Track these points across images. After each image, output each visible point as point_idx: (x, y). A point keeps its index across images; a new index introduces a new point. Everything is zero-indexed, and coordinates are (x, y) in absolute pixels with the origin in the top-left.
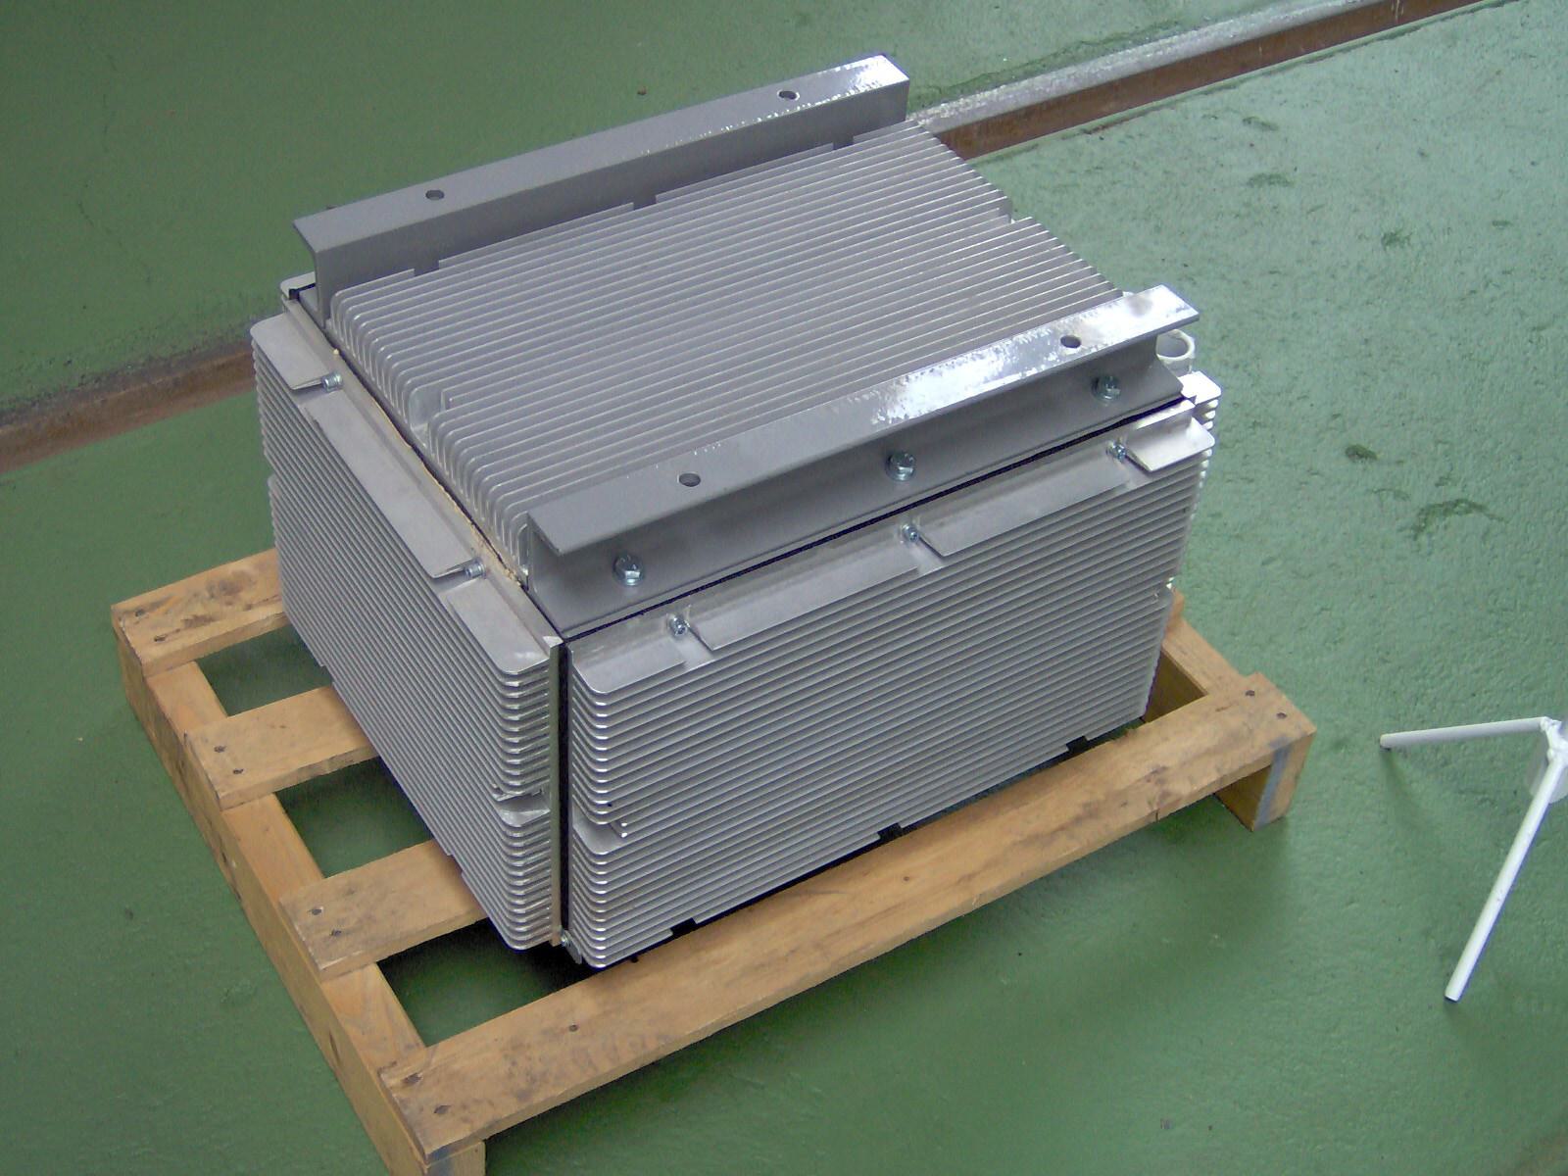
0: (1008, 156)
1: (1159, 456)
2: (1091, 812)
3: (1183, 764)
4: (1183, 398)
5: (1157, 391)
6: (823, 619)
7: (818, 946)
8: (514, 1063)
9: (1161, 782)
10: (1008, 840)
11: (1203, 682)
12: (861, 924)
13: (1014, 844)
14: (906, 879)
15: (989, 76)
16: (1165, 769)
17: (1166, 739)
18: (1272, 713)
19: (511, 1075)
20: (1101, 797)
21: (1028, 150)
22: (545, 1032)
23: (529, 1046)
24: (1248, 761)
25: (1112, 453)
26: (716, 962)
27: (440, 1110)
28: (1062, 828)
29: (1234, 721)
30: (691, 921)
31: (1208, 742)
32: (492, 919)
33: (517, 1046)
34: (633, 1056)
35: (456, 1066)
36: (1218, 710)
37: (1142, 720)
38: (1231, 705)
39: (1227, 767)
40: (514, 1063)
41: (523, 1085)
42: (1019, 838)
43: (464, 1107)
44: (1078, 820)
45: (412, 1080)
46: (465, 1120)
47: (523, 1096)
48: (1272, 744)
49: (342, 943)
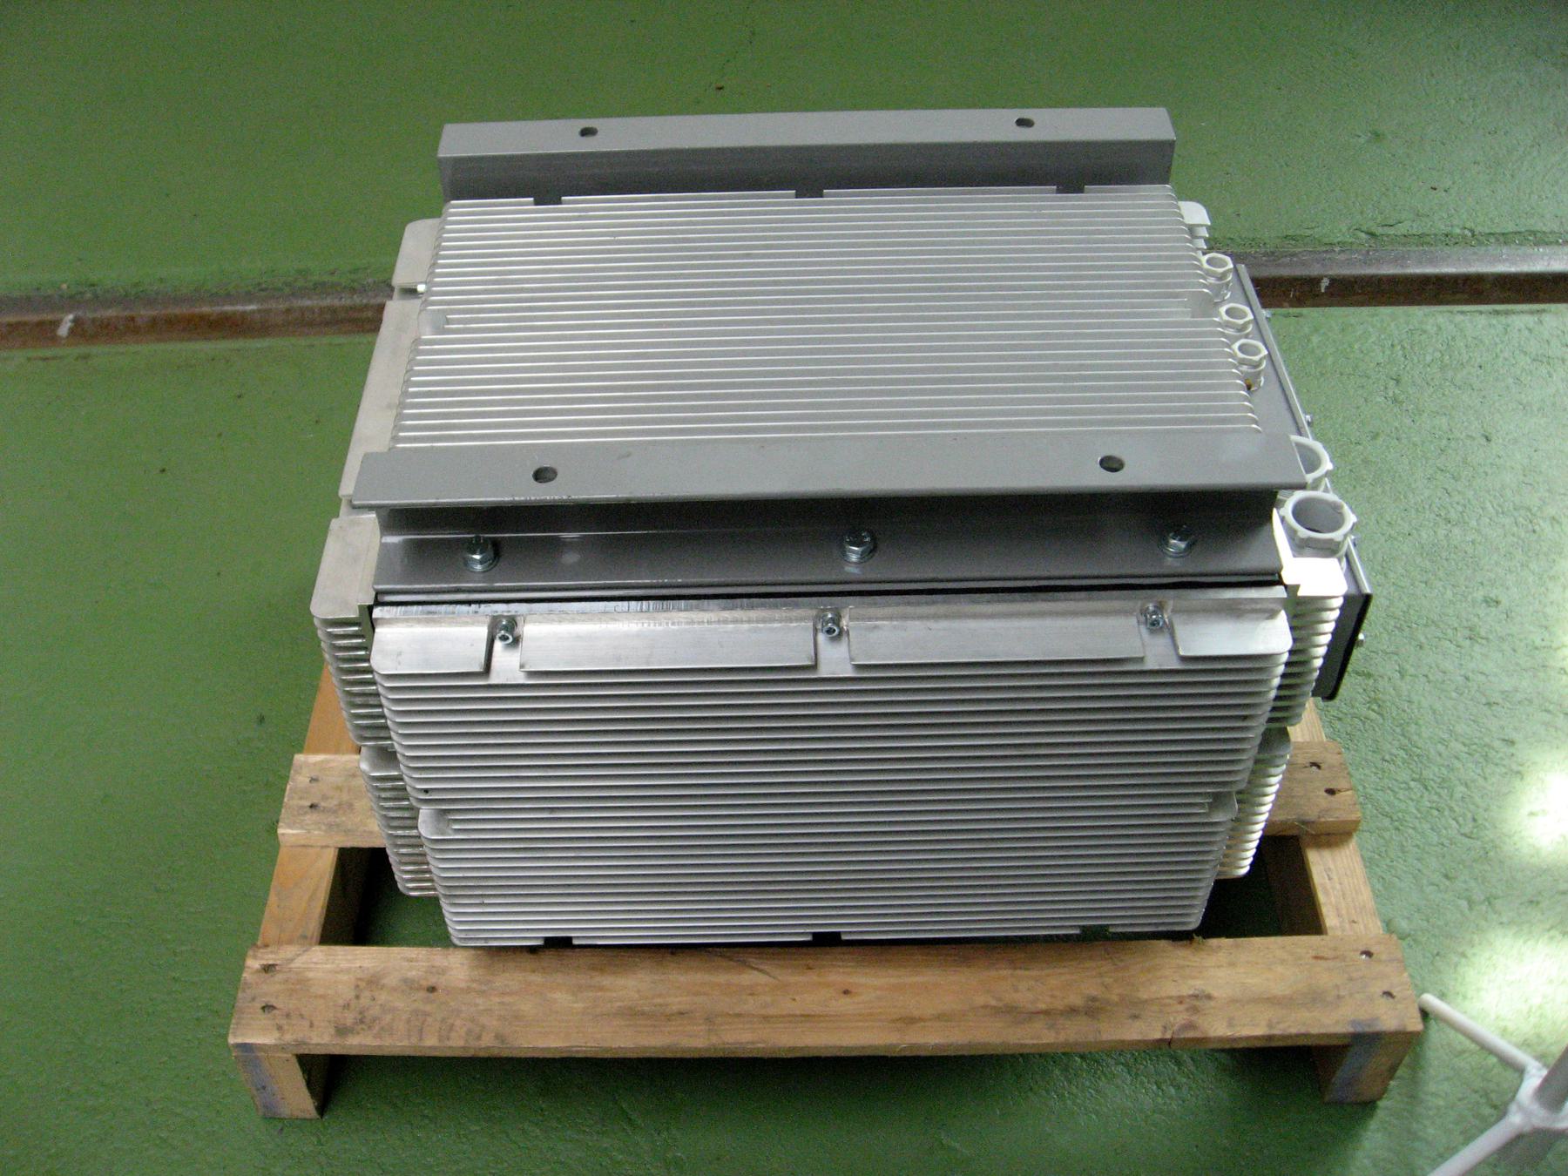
0: (1507, 313)
1: (1214, 637)
2: (1093, 1009)
3: (1233, 1001)
4: (1280, 582)
5: (1248, 559)
6: (1034, 699)
7: (709, 1020)
8: (357, 997)
9: (1195, 1010)
10: (980, 1000)
11: (1330, 919)
12: (766, 1018)
13: (985, 1007)
14: (846, 992)
15: (1534, 233)
16: (1209, 997)
17: (1232, 964)
18: (1377, 988)
19: (347, 1006)
20: (1115, 998)
21: (1532, 313)
22: (405, 981)
23: (383, 987)
24: (1314, 1031)
25: (1144, 612)
26: (601, 989)
27: (267, 1008)
28: (1047, 1013)
29: (1326, 978)
30: (570, 939)
31: (1279, 989)
32: (349, 844)
33: (373, 981)
34: (461, 1043)
35: (310, 975)
36: (1316, 958)
37: (1180, 937)
38: (1335, 958)
39: (1282, 1026)
40: (357, 997)
41: (349, 1022)
42: (993, 1003)
43: (288, 1016)
44: (1072, 1011)
45: (268, 969)
46: (280, 1028)
47: (342, 1031)
48: (1353, 1022)
49: (311, 817)
